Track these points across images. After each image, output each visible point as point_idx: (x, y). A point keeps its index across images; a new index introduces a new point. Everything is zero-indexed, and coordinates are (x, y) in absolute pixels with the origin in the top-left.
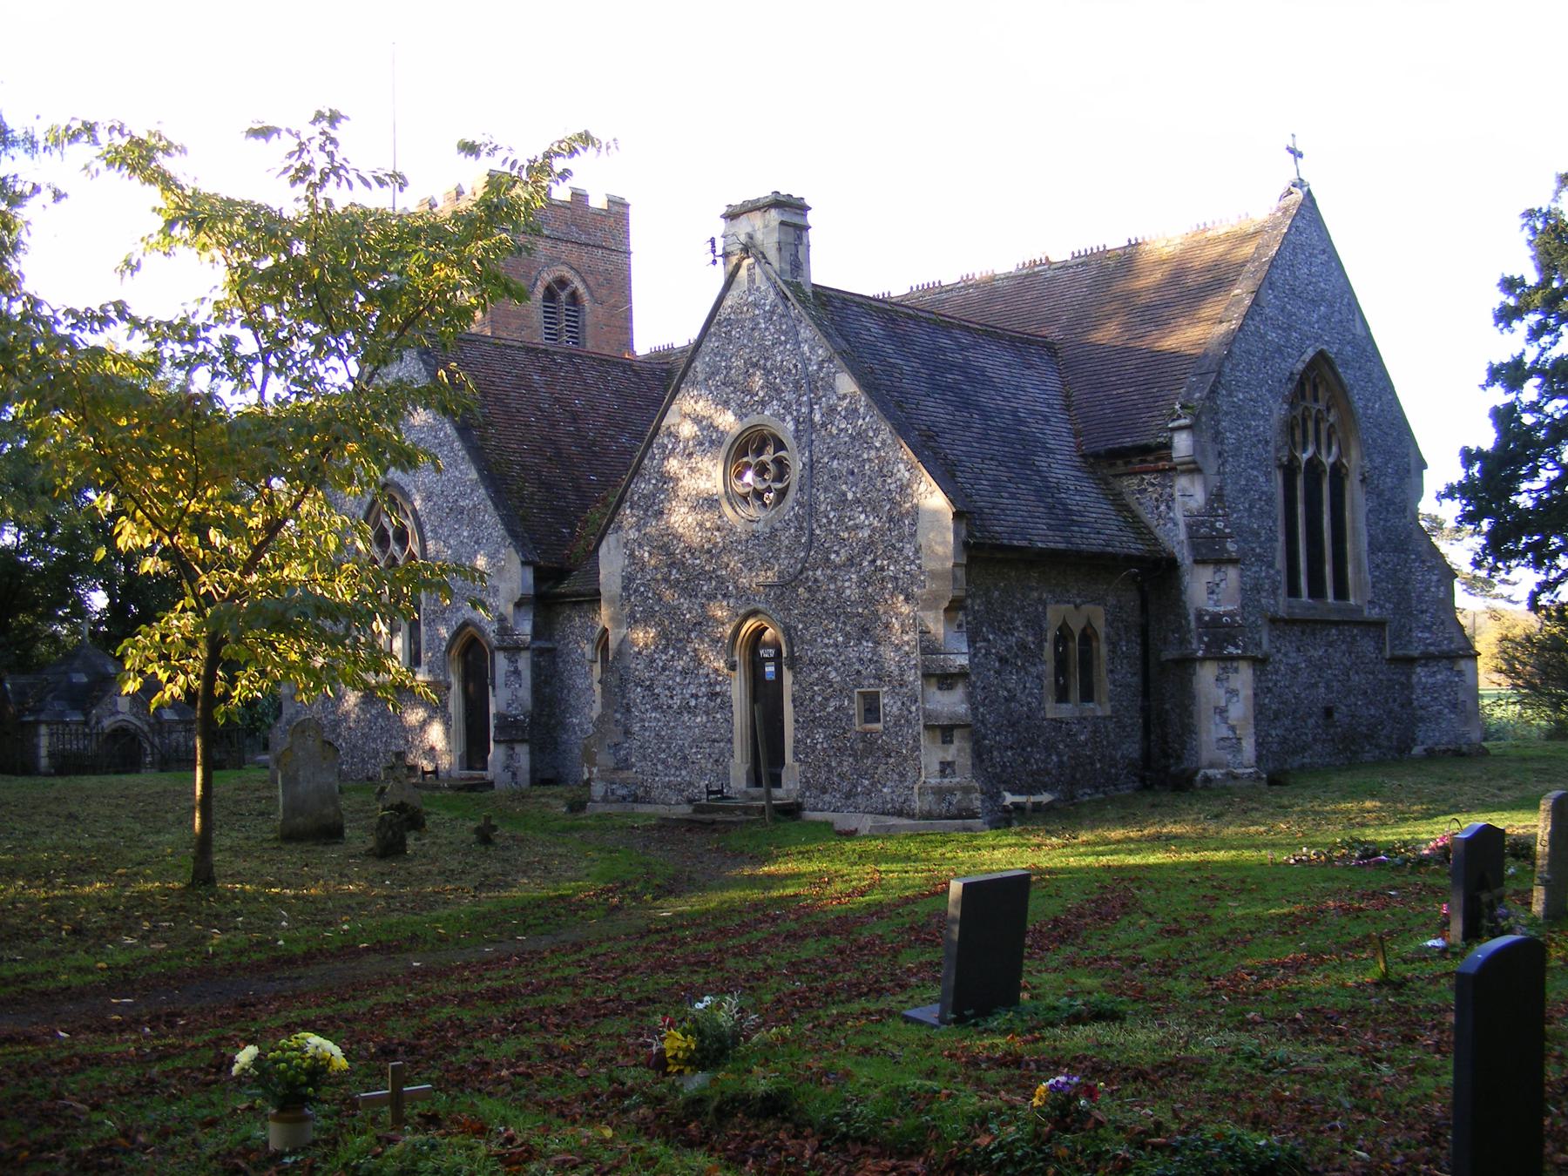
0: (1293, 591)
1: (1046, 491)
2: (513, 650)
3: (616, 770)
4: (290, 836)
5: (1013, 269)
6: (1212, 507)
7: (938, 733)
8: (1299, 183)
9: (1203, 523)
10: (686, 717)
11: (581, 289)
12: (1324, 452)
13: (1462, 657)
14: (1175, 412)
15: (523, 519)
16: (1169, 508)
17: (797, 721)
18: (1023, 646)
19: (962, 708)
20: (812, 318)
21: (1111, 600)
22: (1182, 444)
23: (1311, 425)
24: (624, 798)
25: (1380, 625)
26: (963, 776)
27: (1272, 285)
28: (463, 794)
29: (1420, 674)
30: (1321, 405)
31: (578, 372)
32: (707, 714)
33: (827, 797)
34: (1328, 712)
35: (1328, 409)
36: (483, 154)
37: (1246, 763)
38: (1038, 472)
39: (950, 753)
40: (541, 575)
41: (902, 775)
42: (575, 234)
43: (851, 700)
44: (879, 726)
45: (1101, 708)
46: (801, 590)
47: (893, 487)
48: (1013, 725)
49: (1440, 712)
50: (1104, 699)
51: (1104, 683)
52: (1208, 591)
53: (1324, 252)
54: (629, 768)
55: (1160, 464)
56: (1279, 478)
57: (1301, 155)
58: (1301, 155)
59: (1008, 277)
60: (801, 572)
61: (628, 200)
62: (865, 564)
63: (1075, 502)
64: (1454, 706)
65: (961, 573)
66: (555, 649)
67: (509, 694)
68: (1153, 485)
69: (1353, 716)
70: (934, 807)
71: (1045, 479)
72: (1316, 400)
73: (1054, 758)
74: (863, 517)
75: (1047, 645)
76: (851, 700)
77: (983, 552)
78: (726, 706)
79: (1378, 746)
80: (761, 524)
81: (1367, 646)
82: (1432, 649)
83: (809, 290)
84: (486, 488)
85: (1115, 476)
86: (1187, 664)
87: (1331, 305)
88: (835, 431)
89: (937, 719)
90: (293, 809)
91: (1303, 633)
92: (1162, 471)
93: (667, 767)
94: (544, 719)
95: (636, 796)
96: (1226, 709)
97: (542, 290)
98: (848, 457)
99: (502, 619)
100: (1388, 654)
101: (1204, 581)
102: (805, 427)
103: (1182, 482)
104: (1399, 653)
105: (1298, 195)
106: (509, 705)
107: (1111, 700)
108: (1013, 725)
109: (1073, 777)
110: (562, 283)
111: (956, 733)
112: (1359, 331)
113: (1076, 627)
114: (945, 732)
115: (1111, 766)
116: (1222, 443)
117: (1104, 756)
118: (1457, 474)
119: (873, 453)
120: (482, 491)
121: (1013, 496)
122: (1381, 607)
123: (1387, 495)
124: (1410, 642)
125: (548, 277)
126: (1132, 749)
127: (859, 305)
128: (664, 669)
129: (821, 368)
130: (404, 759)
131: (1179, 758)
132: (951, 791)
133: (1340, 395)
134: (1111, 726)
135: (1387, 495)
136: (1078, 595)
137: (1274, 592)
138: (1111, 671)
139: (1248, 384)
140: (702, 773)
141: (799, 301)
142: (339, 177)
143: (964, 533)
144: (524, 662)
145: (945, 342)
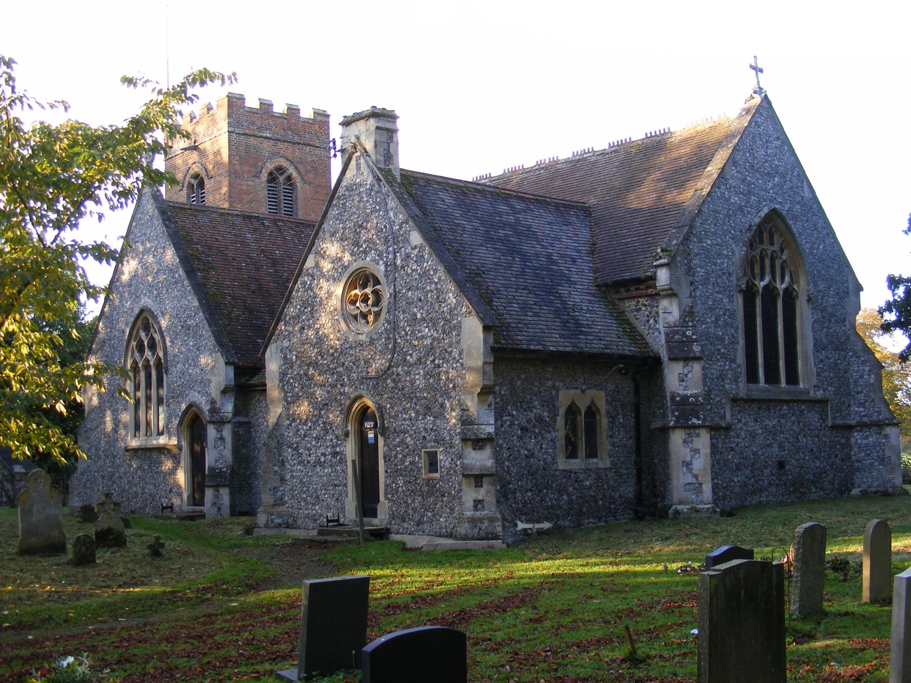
0: (752, 377)
1: (563, 311)
2: (220, 423)
3: (274, 505)
4: (27, 551)
5: (570, 155)
6: (684, 321)
7: (472, 480)
8: (759, 91)
9: (677, 332)
10: (318, 469)
11: (295, 174)
12: (778, 281)
13: (888, 425)
14: (657, 254)
15: (230, 333)
16: (656, 321)
17: (386, 472)
18: (540, 419)
19: (490, 463)
20: (395, 193)
21: (611, 387)
22: (663, 277)
23: (767, 262)
24: (280, 525)
25: (823, 402)
26: (490, 510)
27: (735, 164)
28: (187, 523)
29: (857, 437)
30: (776, 248)
31: (280, 231)
32: (331, 466)
33: (405, 525)
34: (781, 465)
35: (782, 250)
36: (139, 85)
37: (705, 500)
38: (560, 297)
39: (481, 494)
40: (240, 372)
41: (452, 509)
42: (290, 136)
43: (420, 456)
44: (437, 475)
45: (603, 462)
46: (389, 381)
47: (445, 309)
48: (533, 474)
49: (872, 464)
50: (604, 456)
51: (604, 444)
52: (680, 380)
53: (778, 139)
54: (283, 504)
55: (649, 291)
56: (739, 300)
57: (761, 71)
58: (761, 71)
59: (567, 162)
60: (389, 369)
61: (328, 112)
62: (428, 362)
63: (585, 318)
64: (882, 460)
65: (489, 369)
66: (250, 423)
67: (218, 452)
68: (645, 305)
69: (801, 467)
70: (469, 531)
71: (564, 303)
72: (772, 244)
73: (565, 497)
74: (427, 330)
75: (559, 418)
76: (420, 456)
77: (504, 355)
78: (343, 461)
79: (822, 489)
80: (364, 335)
81: (813, 418)
82: (865, 419)
83: (397, 175)
84: (204, 312)
85: (620, 299)
86: (665, 431)
87: (783, 176)
88: (409, 272)
89: (471, 470)
90: (28, 533)
91: (759, 408)
92: (651, 296)
93: (307, 504)
94: (242, 471)
95: (287, 523)
96: (690, 460)
97: (266, 175)
98: (418, 289)
99: (213, 402)
100: (830, 423)
101: (676, 373)
102: (392, 268)
103: (664, 303)
104: (839, 422)
105: (758, 99)
106: (217, 461)
107: (610, 456)
108: (533, 474)
109: (581, 511)
110: (280, 170)
111: (485, 480)
112: (807, 194)
113: (583, 406)
114: (478, 479)
115: (610, 503)
116: (693, 275)
117: (604, 496)
118: (887, 296)
119: (433, 286)
120: (201, 314)
121: (536, 315)
122: (824, 390)
123: (830, 310)
124: (849, 414)
125: (270, 166)
126: (628, 490)
127: (438, 183)
128: (305, 436)
129: (401, 228)
130: (110, 498)
131: (663, 497)
132: (481, 520)
133: (790, 240)
134: (610, 475)
135: (830, 310)
136: (584, 383)
137: (736, 381)
138: (611, 436)
139: (715, 233)
140: (328, 508)
141: (388, 182)
142: (22, 102)
143: (491, 341)
144: (227, 432)
145: (503, 208)
